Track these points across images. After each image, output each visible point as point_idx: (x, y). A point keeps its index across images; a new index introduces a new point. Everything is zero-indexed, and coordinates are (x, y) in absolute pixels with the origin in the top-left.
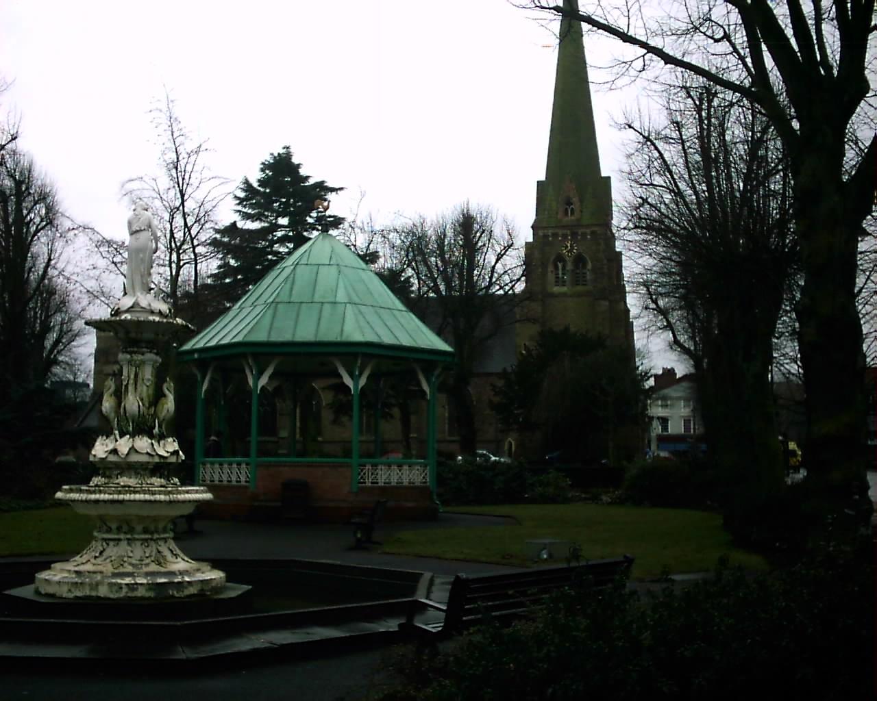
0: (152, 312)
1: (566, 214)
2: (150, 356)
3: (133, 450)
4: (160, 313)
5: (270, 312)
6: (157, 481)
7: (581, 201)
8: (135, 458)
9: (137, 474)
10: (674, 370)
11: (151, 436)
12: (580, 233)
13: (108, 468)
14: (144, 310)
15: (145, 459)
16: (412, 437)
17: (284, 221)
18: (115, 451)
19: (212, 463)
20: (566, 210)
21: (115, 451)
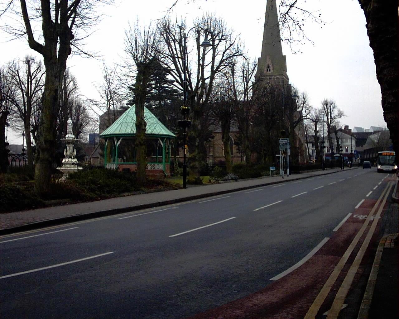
0: (71, 138)
1: (268, 71)
2: (71, 145)
3: (68, 161)
4: (73, 138)
5: (121, 125)
6: (73, 166)
7: (273, 65)
8: (68, 162)
9: (69, 165)
10: (336, 127)
11: (72, 158)
12: (272, 78)
13: (65, 164)
14: (70, 137)
15: (70, 162)
16: (177, 157)
17: (153, 82)
18: (66, 161)
19: (108, 164)
20: (268, 69)
21: (66, 161)
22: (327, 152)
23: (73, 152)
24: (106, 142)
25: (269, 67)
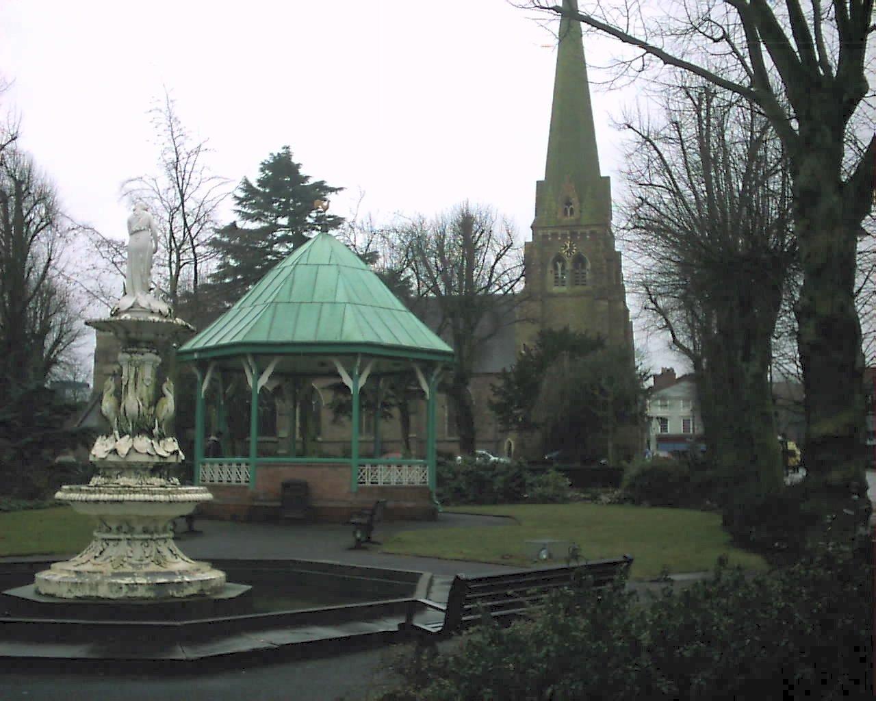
3: (133, 449)
6: (156, 481)
8: (134, 458)
9: (137, 474)
11: (151, 436)
12: (579, 233)
14: (143, 310)
15: (145, 459)
18: (115, 451)
19: (212, 463)
20: (566, 209)
22: (682, 430)
23: (159, 395)
24: (204, 377)
25: (571, 204)
